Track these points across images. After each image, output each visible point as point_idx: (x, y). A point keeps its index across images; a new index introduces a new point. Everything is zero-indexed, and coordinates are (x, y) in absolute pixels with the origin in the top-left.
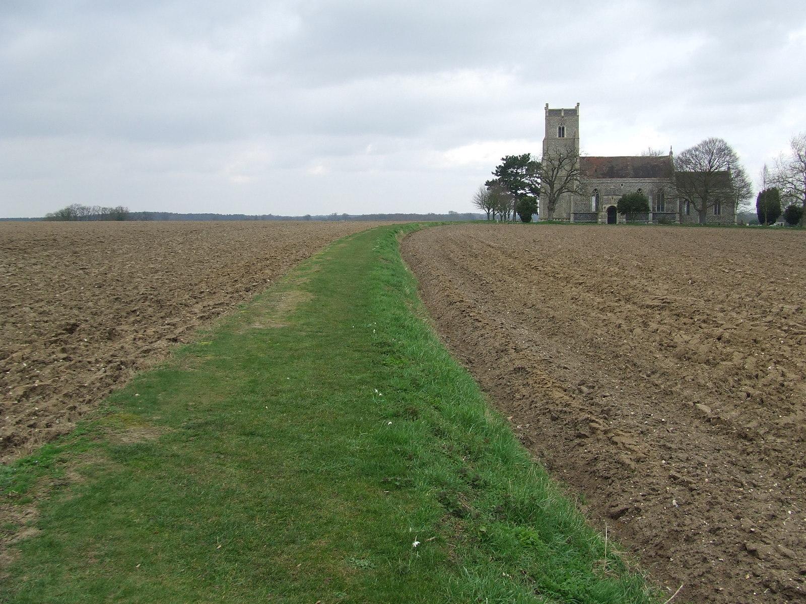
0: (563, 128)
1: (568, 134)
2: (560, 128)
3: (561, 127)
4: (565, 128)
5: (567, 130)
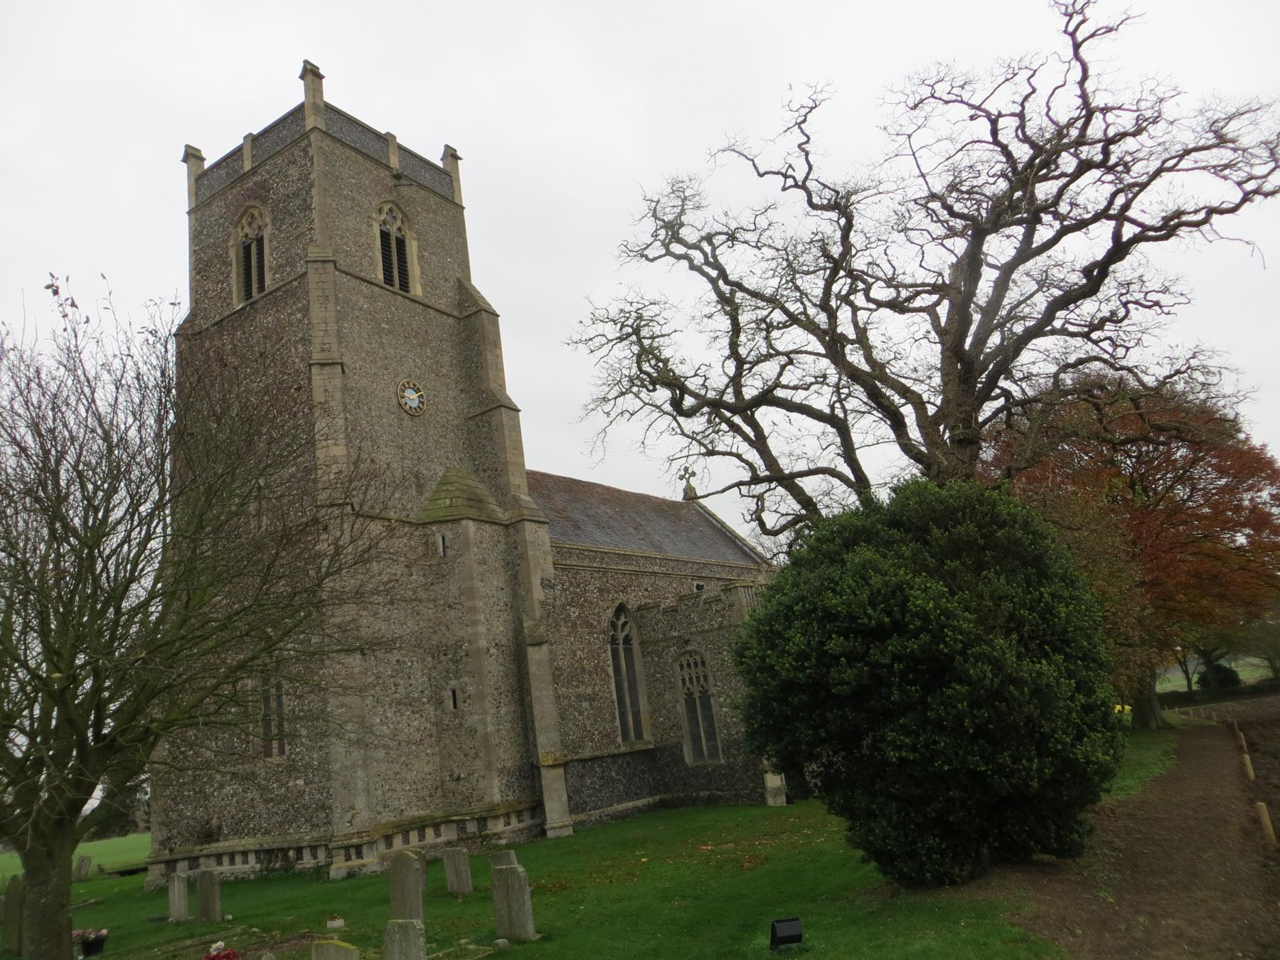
0: (401, 243)
1: (428, 284)
2: (385, 236)
3: (393, 230)
4: (412, 247)
5: (421, 258)
